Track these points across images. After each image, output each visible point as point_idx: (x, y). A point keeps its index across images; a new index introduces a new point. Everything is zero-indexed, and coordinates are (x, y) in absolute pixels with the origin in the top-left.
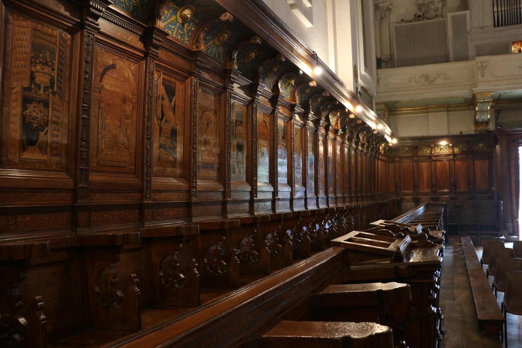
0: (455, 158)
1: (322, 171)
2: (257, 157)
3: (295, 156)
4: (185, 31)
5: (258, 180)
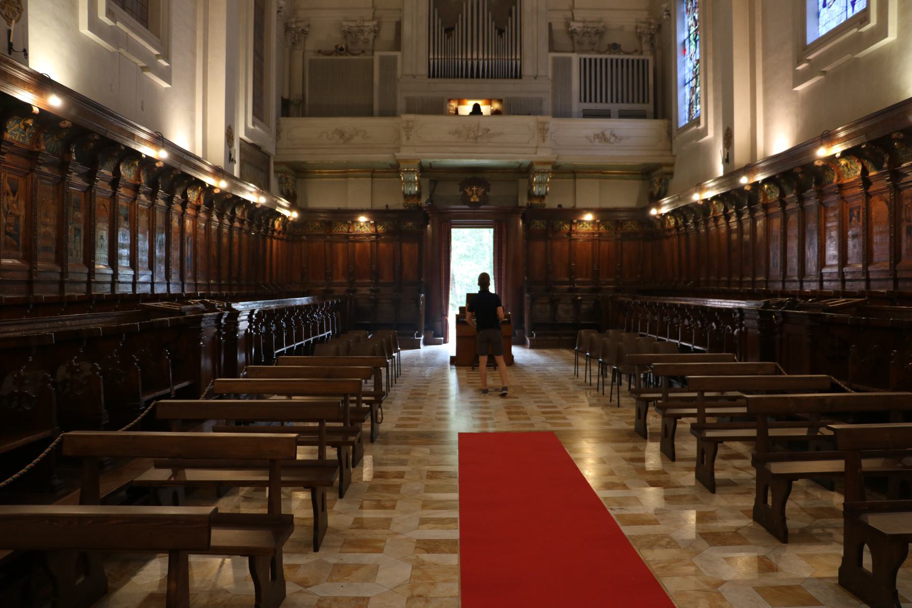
0: (379, 240)
1: (175, 254)
2: (94, 240)
3: (140, 236)
4: (26, 134)
5: (96, 263)
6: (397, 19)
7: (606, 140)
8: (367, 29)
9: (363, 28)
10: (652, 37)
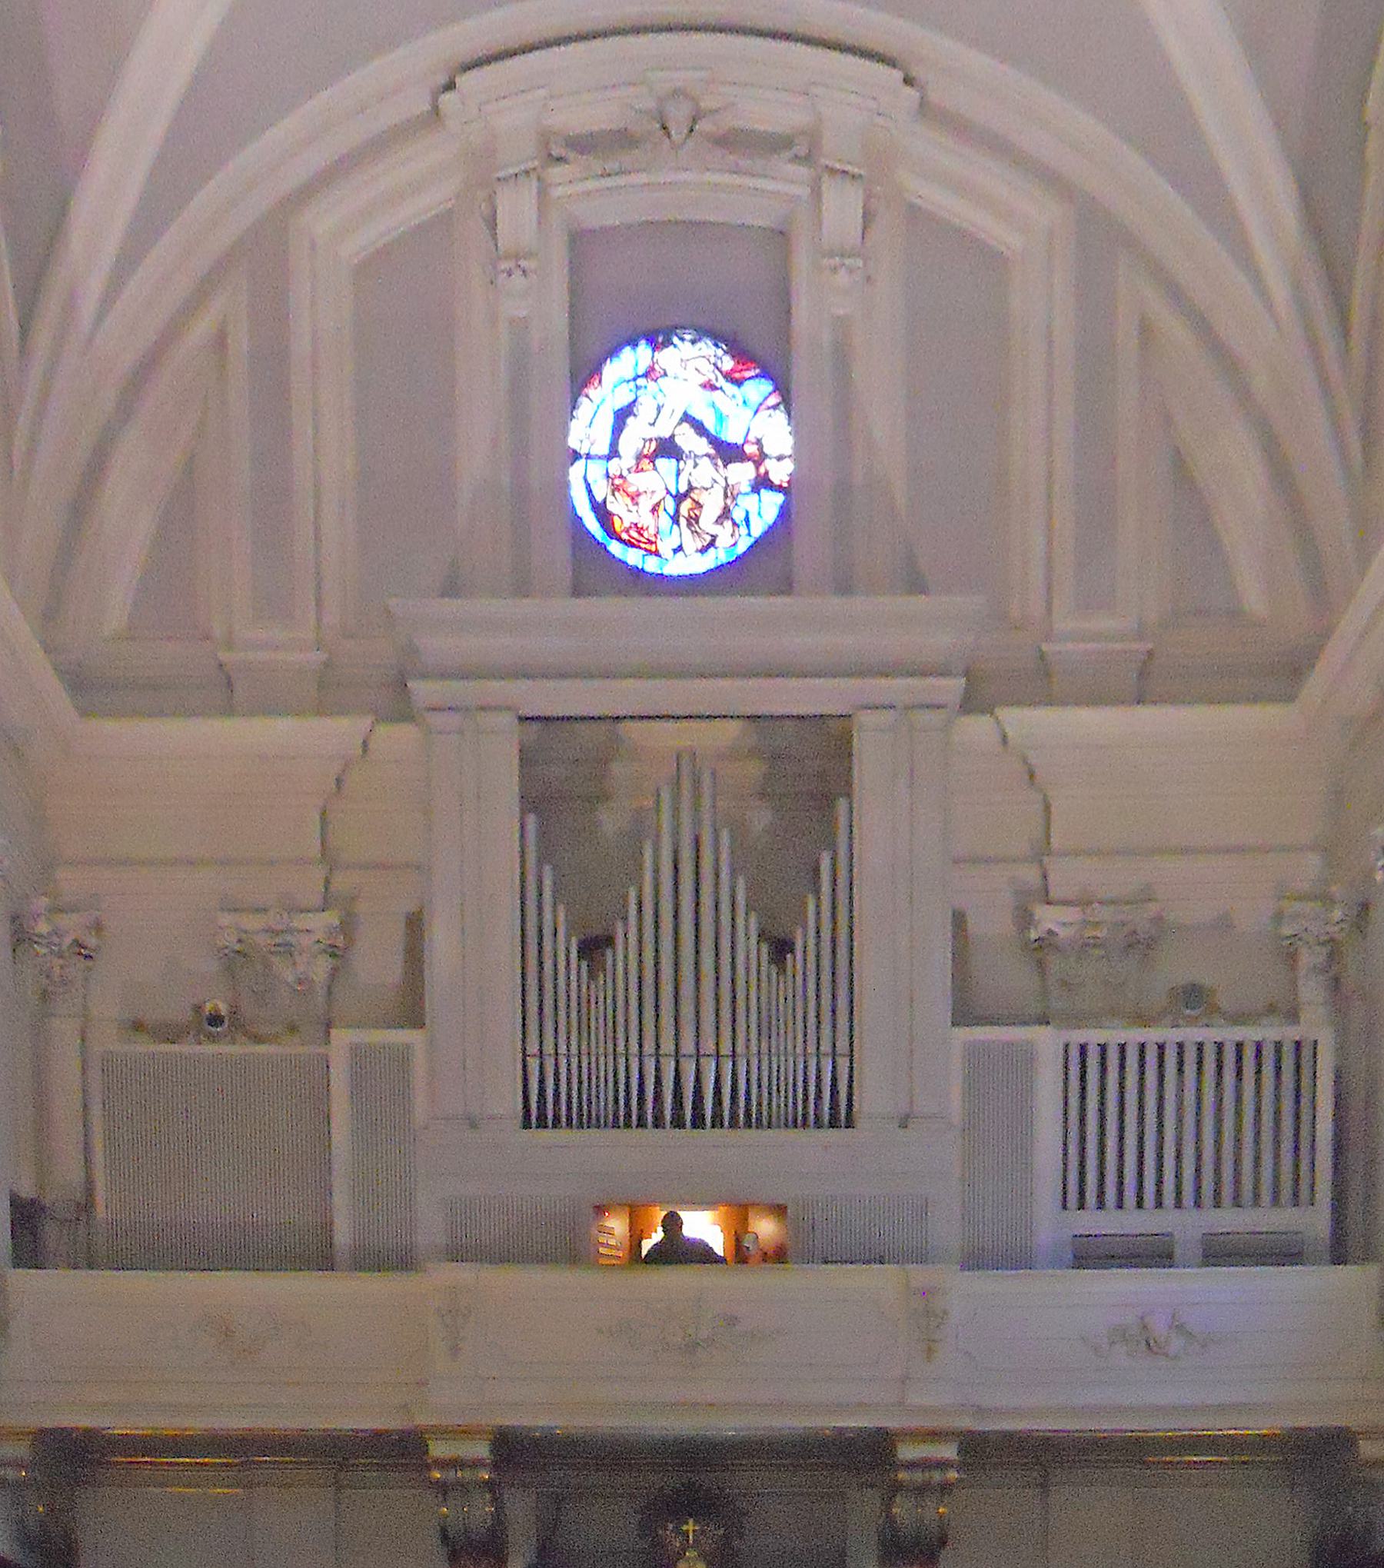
6: (412, 907)
7: (1151, 1346)
8: (306, 941)
9: (289, 938)
10: (1334, 950)
